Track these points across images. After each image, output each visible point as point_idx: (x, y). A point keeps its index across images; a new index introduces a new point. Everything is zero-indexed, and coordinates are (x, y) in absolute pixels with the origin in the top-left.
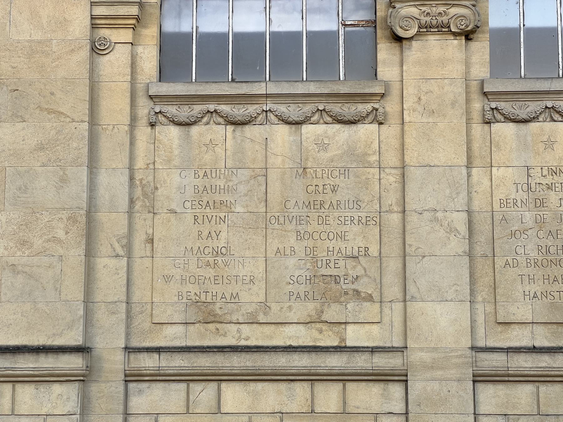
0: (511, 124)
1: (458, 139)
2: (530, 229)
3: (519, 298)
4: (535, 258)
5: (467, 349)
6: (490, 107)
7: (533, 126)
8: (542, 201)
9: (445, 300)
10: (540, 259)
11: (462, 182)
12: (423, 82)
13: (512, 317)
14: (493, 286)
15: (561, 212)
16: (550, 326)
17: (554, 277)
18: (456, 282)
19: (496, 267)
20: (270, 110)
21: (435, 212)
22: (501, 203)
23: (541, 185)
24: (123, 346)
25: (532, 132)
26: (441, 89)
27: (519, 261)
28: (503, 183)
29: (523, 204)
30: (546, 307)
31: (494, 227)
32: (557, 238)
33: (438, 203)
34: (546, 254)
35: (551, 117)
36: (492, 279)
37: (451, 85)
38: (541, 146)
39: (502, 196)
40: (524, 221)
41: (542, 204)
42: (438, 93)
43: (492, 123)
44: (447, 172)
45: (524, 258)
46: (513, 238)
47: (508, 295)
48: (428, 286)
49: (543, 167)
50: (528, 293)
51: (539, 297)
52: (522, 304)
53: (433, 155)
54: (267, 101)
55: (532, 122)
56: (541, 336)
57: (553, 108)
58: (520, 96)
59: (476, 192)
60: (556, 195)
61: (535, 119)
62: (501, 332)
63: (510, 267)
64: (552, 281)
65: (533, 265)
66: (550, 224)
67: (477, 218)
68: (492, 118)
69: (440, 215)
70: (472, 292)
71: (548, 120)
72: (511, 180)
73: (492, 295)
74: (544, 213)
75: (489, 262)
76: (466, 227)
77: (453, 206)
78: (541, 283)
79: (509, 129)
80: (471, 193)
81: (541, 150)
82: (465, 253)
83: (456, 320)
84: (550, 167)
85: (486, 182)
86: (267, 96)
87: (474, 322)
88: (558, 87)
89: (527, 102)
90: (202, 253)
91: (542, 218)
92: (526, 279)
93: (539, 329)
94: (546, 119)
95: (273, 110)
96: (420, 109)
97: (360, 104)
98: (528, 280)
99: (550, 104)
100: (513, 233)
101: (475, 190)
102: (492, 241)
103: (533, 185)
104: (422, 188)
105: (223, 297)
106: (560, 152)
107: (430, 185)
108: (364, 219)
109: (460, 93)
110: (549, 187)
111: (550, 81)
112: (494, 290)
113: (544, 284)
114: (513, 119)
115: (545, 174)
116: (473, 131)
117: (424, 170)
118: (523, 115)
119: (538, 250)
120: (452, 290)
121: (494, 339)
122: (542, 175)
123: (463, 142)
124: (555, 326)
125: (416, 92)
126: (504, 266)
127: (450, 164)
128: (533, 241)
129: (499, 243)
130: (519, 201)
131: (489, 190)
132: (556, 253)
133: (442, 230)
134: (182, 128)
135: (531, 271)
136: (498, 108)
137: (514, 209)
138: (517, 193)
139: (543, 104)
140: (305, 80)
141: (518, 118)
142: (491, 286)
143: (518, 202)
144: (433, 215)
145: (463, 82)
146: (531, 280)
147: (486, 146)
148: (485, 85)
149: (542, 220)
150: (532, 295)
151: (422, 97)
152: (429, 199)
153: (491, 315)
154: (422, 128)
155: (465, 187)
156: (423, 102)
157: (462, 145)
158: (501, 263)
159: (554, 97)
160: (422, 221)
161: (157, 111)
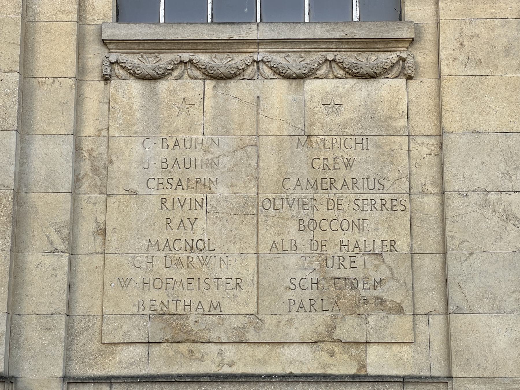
9: (503, 313)
12: (466, 23)
21: (485, 193)
24: (61, 375)
26: (490, 32)
37: (503, 26)
48: (479, 293)
53: (481, 118)
54: (258, 49)
77: (510, 185)
90: (172, 248)
96: (463, 58)
105: (301, 306)
107: (478, 158)
117: (469, 138)
120: (512, 299)
125: (457, 37)
127: (504, 130)
133: (496, 219)
134: (146, 83)
144: (483, 197)
151: (465, 43)
152: (477, 176)
154: (466, 82)
156: (466, 49)
160: (468, 205)
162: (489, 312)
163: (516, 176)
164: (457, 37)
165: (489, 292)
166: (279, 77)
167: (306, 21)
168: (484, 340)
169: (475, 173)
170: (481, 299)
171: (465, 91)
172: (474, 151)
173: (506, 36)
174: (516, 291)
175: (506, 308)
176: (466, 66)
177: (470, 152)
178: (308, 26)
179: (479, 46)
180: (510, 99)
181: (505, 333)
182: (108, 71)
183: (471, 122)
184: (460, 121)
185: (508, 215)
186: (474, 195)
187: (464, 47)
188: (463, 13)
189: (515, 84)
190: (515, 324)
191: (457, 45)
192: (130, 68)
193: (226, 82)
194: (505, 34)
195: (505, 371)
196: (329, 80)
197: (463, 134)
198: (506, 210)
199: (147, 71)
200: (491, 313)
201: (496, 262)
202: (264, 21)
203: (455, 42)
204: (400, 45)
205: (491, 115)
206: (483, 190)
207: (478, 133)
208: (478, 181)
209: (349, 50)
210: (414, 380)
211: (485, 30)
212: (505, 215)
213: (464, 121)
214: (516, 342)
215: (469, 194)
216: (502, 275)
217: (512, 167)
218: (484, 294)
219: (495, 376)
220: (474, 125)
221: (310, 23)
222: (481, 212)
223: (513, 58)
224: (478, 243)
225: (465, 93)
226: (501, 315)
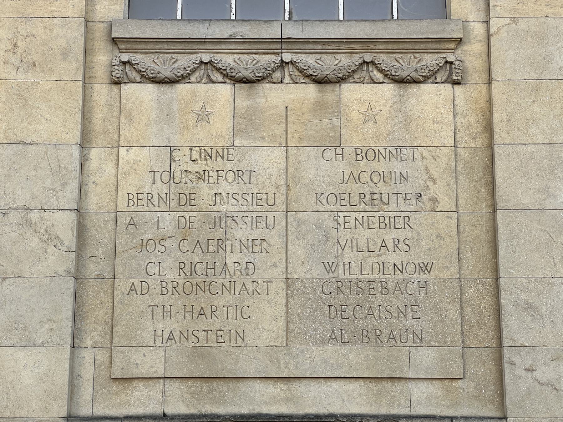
0: (150, 85)
1: (69, 105)
2: (169, 237)
3: (146, 340)
4: (175, 280)
5: (60, 420)
6: (120, 60)
7: (182, 88)
8: (188, 197)
9: (32, 345)
10: (181, 282)
11: (72, 167)
12: (22, 22)
13: (135, 370)
14: (110, 323)
15: (216, 213)
16: (190, 383)
17: (200, 308)
18: (52, 317)
19: (115, 294)
21: (27, 211)
22: (129, 200)
23: (188, 174)
24: (64, 414)
25: (180, 97)
26: (48, 32)
27: (150, 285)
28: (135, 170)
29: (161, 201)
30: (186, 354)
31: (117, 234)
32: (208, 252)
33: (33, 197)
34: (191, 275)
35: (209, 77)
36: (110, 312)
37: (63, 26)
38: (192, 118)
39: (133, 190)
40: (161, 226)
41: (188, 201)
42: (43, 37)
43: (123, 83)
44: (49, 153)
45: (158, 281)
46: (144, 251)
47: (130, 336)
48: (8, 323)
49: (193, 148)
50: (160, 333)
51: (177, 339)
52: (151, 350)
53: (30, 127)
54: (282, 49)
55: (182, 83)
56: (175, 398)
57: (212, 63)
58: (165, 46)
59: (94, 182)
60: (210, 188)
61: (186, 79)
62: (117, 393)
63: (137, 294)
64: (197, 316)
65: (170, 290)
66: (199, 231)
67: (92, 222)
68: (122, 75)
69: (34, 216)
70: (76, 333)
71: (204, 81)
72: (145, 167)
73: (108, 337)
74: (191, 214)
75: (107, 287)
76: (73, 235)
77: (56, 202)
78: (181, 318)
79: (147, 93)
80: (86, 185)
81: (192, 123)
82: (69, 272)
83: (46, 375)
84: (203, 148)
85: (110, 169)
86: (282, 41)
87: (78, 378)
88: (217, 34)
89: (176, 55)
91: (188, 222)
92: (159, 311)
93: (174, 388)
94: (201, 79)
95: (134, 62)
96: (15, 60)
97: (426, 54)
98: (161, 314)
99: (206, 58)
100: (144, 244)
101: (93, 180)
102: (113, 256)
103: (177, 174)
104: (10, 176)
106: (219, 126)
107: (23, 172)
109: (76, 38)
110: (200, 177)
111: (206, 24)
112: (110, 329)
113: (185, 319)
114: (153, 78)
115: (195, 157)
116: (95, 94)
117: (15, 149)
118: (166, 72)
119: (180, 268)
120: (44, 329)
121: (106, 404)
122: (191, 158)
123: (77, 110)
124: (198, 383)
125: (11, 36)
126: (127, 293)
127: (54, 141)
128: (173, 255)
129: (124, 258)
130: (156, 197)
131: (114, 180)
132: (205, 273)
133: (36, 240)
135: (167, 300)
136: (131, 62)
137: (147, 208)
138: (154, 186)
139: (356, 59)
140: (234, 19)
141: (158, 76)
142: (107, 323)
143: (154, 198)
144: (24, 216)
145: (81, 23)
146: (167, 313)
147: (112, 117)
148: (114, 29)
149: (188, 226)
150: (166, 336)
151: (19, 44)
152: (20, 192)
153: (103, 367)
154: (16, 87)
155: (76, 175)
156: (20, 51)
157: (75, 114)
158: (123, 289)
159: (213, 48)
160: (6, 225)
162: (16, 344)
163: (63, 193)
164: (11, 36)
165: (19, 322)
167: (340, 19)
168: (8, 375)
169: (18, 188)
170: (9, 330)
171: (15, 97)
172: (19, 164)
173: (66, 36)
174: (49, 320)
175: (36, 340)
176: (18, 70)
177: (14, 166)
178: (181, 23)
179: (34, 48)
180: (64, 106)
181: (32, 368)
182: (118, 72)
183: (19, 132)
184: (6, 131)
185: (50, 235)
186: (14, 213)
187: (18, 49)
188: (20, 10)
189: (71, 89)
190: (45, 357)
191: (10, 46)
192: (386, 69)
193: (175, 87)
194: (64, 34)
195: (28, 410)
196: (202, 84)
197: (9, 145)
198: (49, 230)
199: (244, 74)
200: (19, 345)
201: (31, 288)
202: (295, 17)
203: (8, 42)
204: (447, 46)
205: (42, 124)
206: (25, 207)
207: (25, 144)
208: (20, 197)
211: (42, 29)
212: (46, 235)
213: (10, 130)
214: (44, 377)
215: (9, 212)
216: (36, 303)
217: (59, 183)
218: (14, 324)
219: (16, 416)
220: (21, 135)
222: (20, 233)
223: (70, 62)
224: (13, 266)
225: (15, 100)
226: (30, 347)
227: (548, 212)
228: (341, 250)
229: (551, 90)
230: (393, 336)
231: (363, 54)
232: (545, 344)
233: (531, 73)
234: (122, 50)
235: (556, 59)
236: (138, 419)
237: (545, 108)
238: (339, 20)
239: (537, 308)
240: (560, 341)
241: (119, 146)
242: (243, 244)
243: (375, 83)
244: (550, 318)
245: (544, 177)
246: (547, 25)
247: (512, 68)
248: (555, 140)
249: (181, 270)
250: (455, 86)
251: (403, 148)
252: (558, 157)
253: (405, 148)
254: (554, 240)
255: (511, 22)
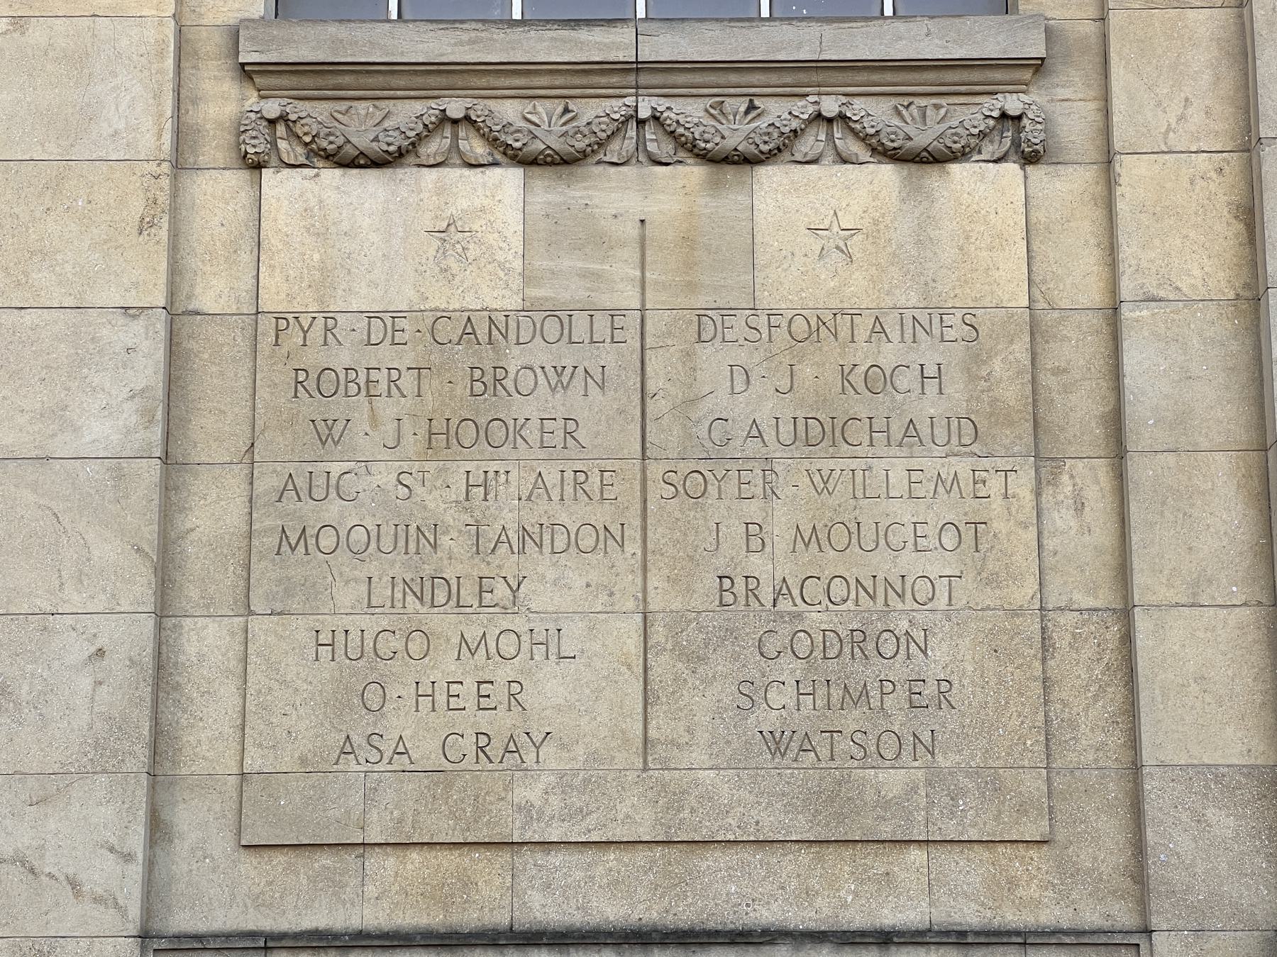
20: (467, 118)
90: (798, 600)
105: (401, 749)
108: (595, 479)
122: (723, 339)
134: (905, 169)
161: (1011, 113)
166: (881, 158)
182: (256, 147)
209: (788, 90)
210: (1095, 939)
221: (402, 25)
227: (57, 465)
228: (803, 546)
229: (90, 184)
230: (353, 748)
231: (348, 103)
232: (18, 768)
233: (47, 144)
234: (262, 92)
235: (108, 113)
236: (862, 935)
237: (73, 225)
238: (389, 21)
239: (9, 686)
240: (55, 759)
241: (258, 312)
242: (528, 534)
243: (845, 162)
244: (36, 708)
245: (56, 384)
246: (94, 35)
247: (4, 133)
248: (90, 299)
249: (750, 593)
250: (1029, 168)
251: (618, 312)
252: (93, 339)
253: (732, 312)
254: (64, 528)
255: (11, 28)
